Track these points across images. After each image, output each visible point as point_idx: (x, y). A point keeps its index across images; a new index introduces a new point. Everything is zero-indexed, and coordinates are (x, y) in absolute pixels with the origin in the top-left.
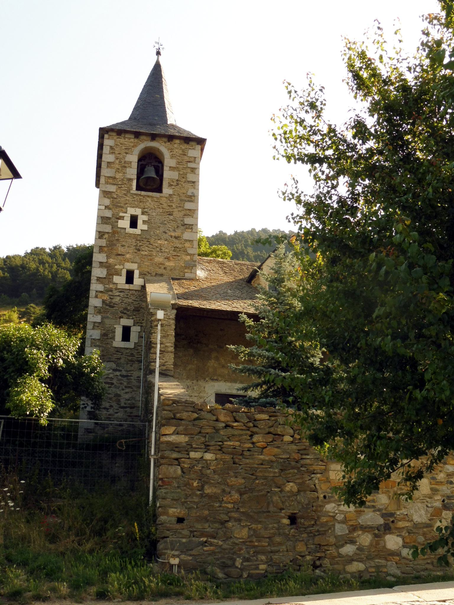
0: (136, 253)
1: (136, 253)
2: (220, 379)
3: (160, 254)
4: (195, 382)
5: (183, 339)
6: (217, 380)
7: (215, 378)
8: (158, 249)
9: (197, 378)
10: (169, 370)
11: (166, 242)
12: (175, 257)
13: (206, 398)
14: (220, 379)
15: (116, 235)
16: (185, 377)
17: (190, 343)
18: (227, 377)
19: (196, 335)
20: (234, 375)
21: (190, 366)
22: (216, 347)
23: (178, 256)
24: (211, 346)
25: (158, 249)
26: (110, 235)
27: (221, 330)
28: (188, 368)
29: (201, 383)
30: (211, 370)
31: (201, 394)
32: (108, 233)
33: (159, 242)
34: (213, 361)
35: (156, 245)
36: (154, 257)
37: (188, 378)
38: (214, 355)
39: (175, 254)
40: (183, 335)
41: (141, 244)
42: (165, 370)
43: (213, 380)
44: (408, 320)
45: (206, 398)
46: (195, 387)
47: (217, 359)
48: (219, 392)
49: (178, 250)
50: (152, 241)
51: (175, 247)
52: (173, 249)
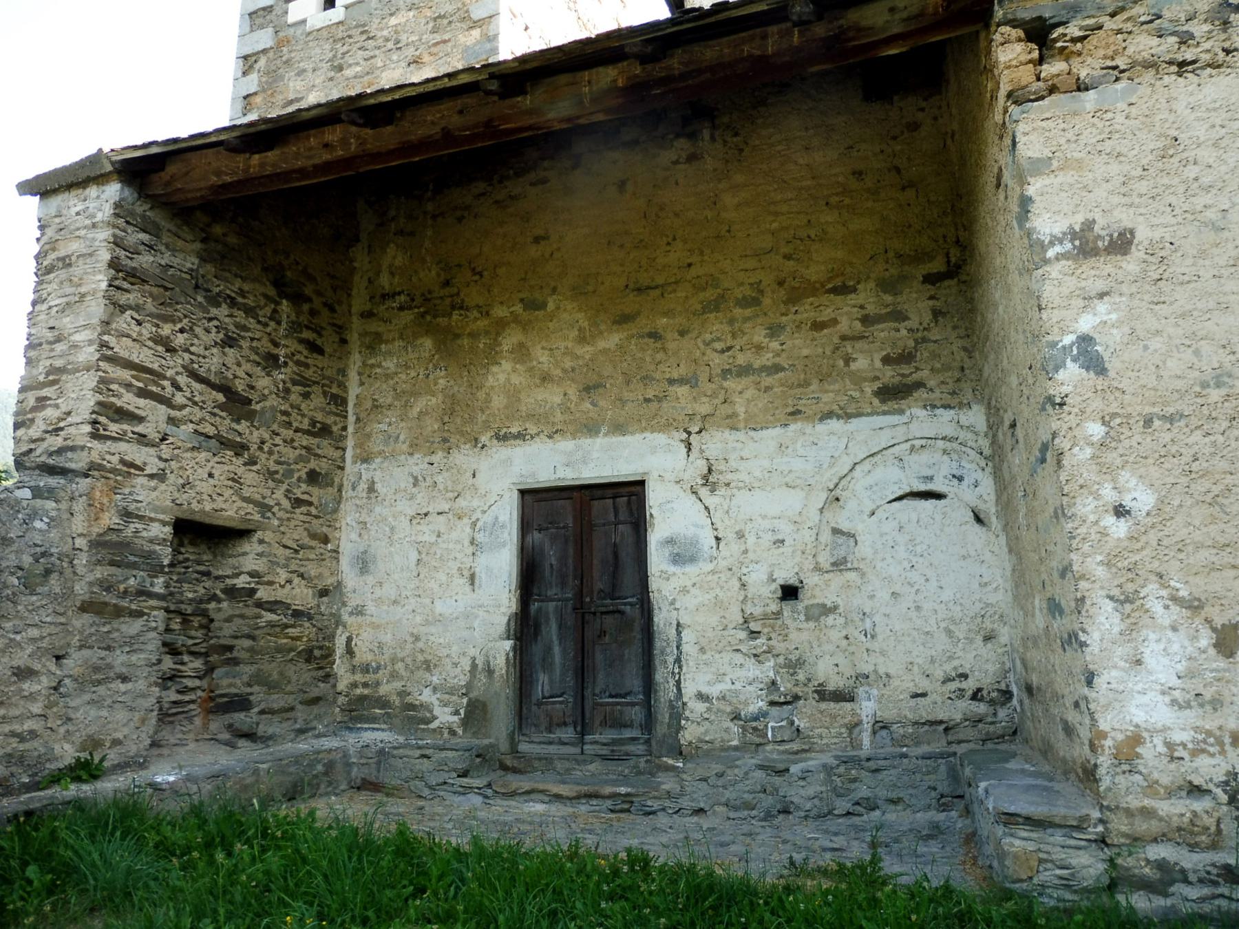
0: (331, 79)
1: (331, 79)
2: (533, 430)
3: (395, 57)
4: (438, 457)
5: (401, 308)
6: (520, 436)
7: (514, 430)
8: (390, 45)
9: (445, 440)
10: (72, 449)
11: (411, 14)
12: (434, 50)
13: (478, 514)
14: (533, 430)
15: (285, 49)
16: (405, 447)
17: (423, 315)
18: (559, 417)
19: (447, 283)
20: (587, 405)
21: (420, 405)
22: (518, 308)
23: (445, 42)
24: (500, 312)
25: (390, 45)
26: (271, 54)
27: (537, 240)
28: (415, 412)
29: (464, 457)
30: (498, 402)
31: (461, 502)
32: (264, 51)
33: (393, 21)
34: (506, 365)
35: (385, 33)
36: (378, 72)
37: (414, 447)
38: (509, 340)
39: (438, 38)
40: (399, 294)
41: (345, 48)
42: (60, 451)
43: (502, 438)
44: (972, 746)
45: (478, 514)
46: (439, 479)
47: (521, 353)
48: (531, 484)
49: (445, 21)
50: (373, 28)
51: (435, 19)
52: (431, 24)
